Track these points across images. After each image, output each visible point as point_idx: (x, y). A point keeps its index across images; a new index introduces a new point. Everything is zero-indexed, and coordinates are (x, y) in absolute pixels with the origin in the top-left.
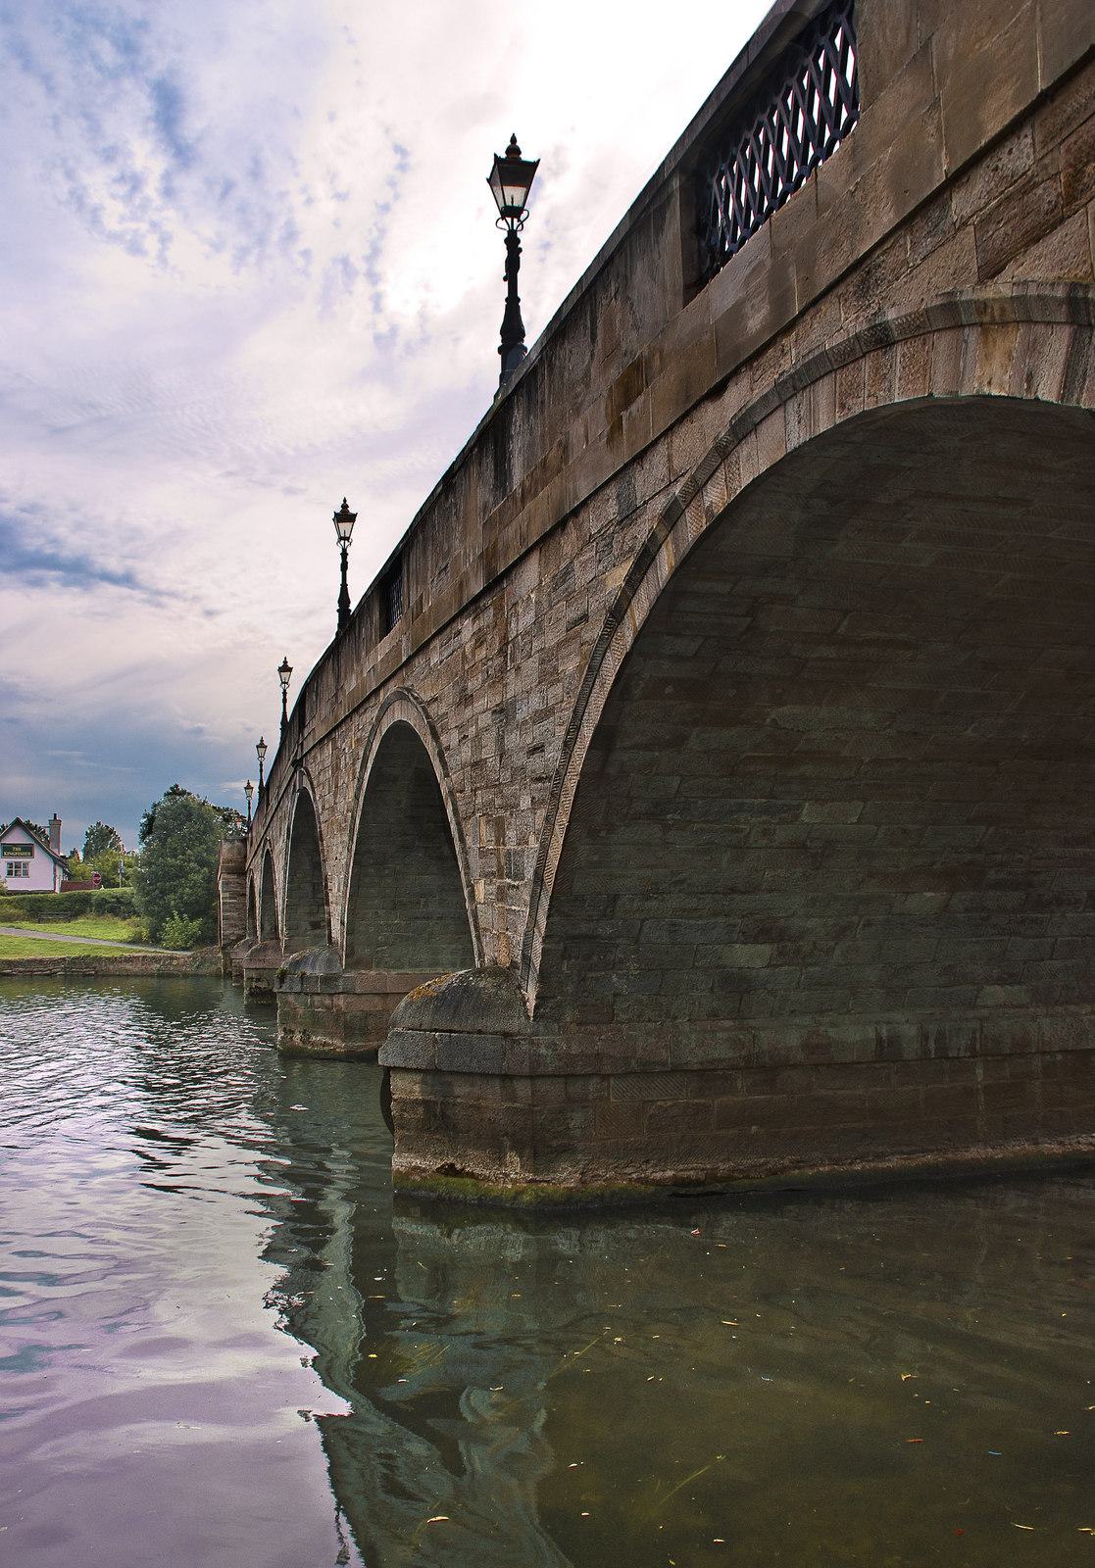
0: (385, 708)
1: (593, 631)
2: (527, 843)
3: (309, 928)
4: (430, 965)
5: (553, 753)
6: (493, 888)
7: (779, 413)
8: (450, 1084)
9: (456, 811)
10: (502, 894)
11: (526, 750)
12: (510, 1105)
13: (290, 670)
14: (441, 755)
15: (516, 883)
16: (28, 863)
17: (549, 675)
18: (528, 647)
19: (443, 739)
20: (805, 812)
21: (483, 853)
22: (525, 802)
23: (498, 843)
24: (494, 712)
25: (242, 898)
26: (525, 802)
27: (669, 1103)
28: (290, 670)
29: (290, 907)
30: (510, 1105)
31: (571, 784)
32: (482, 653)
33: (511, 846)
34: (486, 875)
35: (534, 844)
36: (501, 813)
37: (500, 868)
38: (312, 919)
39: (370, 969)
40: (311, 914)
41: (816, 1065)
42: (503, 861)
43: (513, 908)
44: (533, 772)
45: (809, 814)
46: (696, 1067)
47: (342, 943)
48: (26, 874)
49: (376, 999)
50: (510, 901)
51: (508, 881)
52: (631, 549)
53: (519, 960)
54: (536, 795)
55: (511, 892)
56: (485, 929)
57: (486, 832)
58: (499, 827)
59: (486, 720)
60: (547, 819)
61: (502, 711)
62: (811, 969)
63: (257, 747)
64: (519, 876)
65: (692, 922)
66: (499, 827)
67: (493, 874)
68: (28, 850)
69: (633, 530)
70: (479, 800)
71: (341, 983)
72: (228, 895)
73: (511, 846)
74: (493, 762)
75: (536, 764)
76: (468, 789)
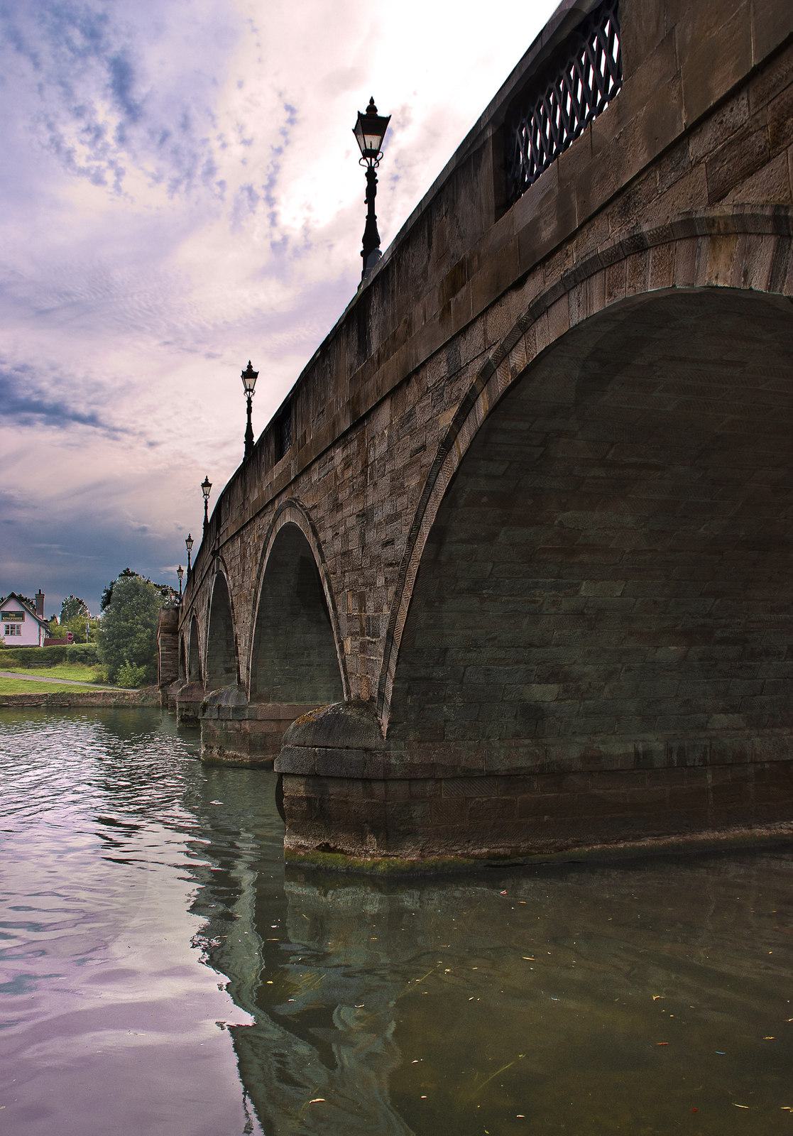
1: (430, 458)
2: (382, 611)
3: (224, 672)
5: (401, 546)
6: (357, 644)
7: (565, 299)
10: (363, 648)
12: (369, 800)
13: (210, 485)
14: (319, 547)
15: (374, 640)
16: (20, 625)
17: (397, 489)
22: (380, 581)
23: (360, 610)
24: (358, 516)
26: (380, 581)
28: (210, 485)
30: (369, 800)
33: (370, 613)
35: (386, 611)
36: (363, 589)
37: (362, 629)
39: (268, 702)
40: (225, 662)
43: (372, 658)
44: (386, 559)
45: (586, 589)
47: (248, 683)
49: (273, 724)
51: (368, 638)
52: (457, 398)
53: (376, 695)
54: (388, 576)
60: (396, 593)
62: (587, 702)
63: (186, 541)
64: (376, 635)
67: (357, 633)
69: (459, 384)
71: (247, 712)
74: (357, 552)
75: (388, 553)
76: (339, 572)
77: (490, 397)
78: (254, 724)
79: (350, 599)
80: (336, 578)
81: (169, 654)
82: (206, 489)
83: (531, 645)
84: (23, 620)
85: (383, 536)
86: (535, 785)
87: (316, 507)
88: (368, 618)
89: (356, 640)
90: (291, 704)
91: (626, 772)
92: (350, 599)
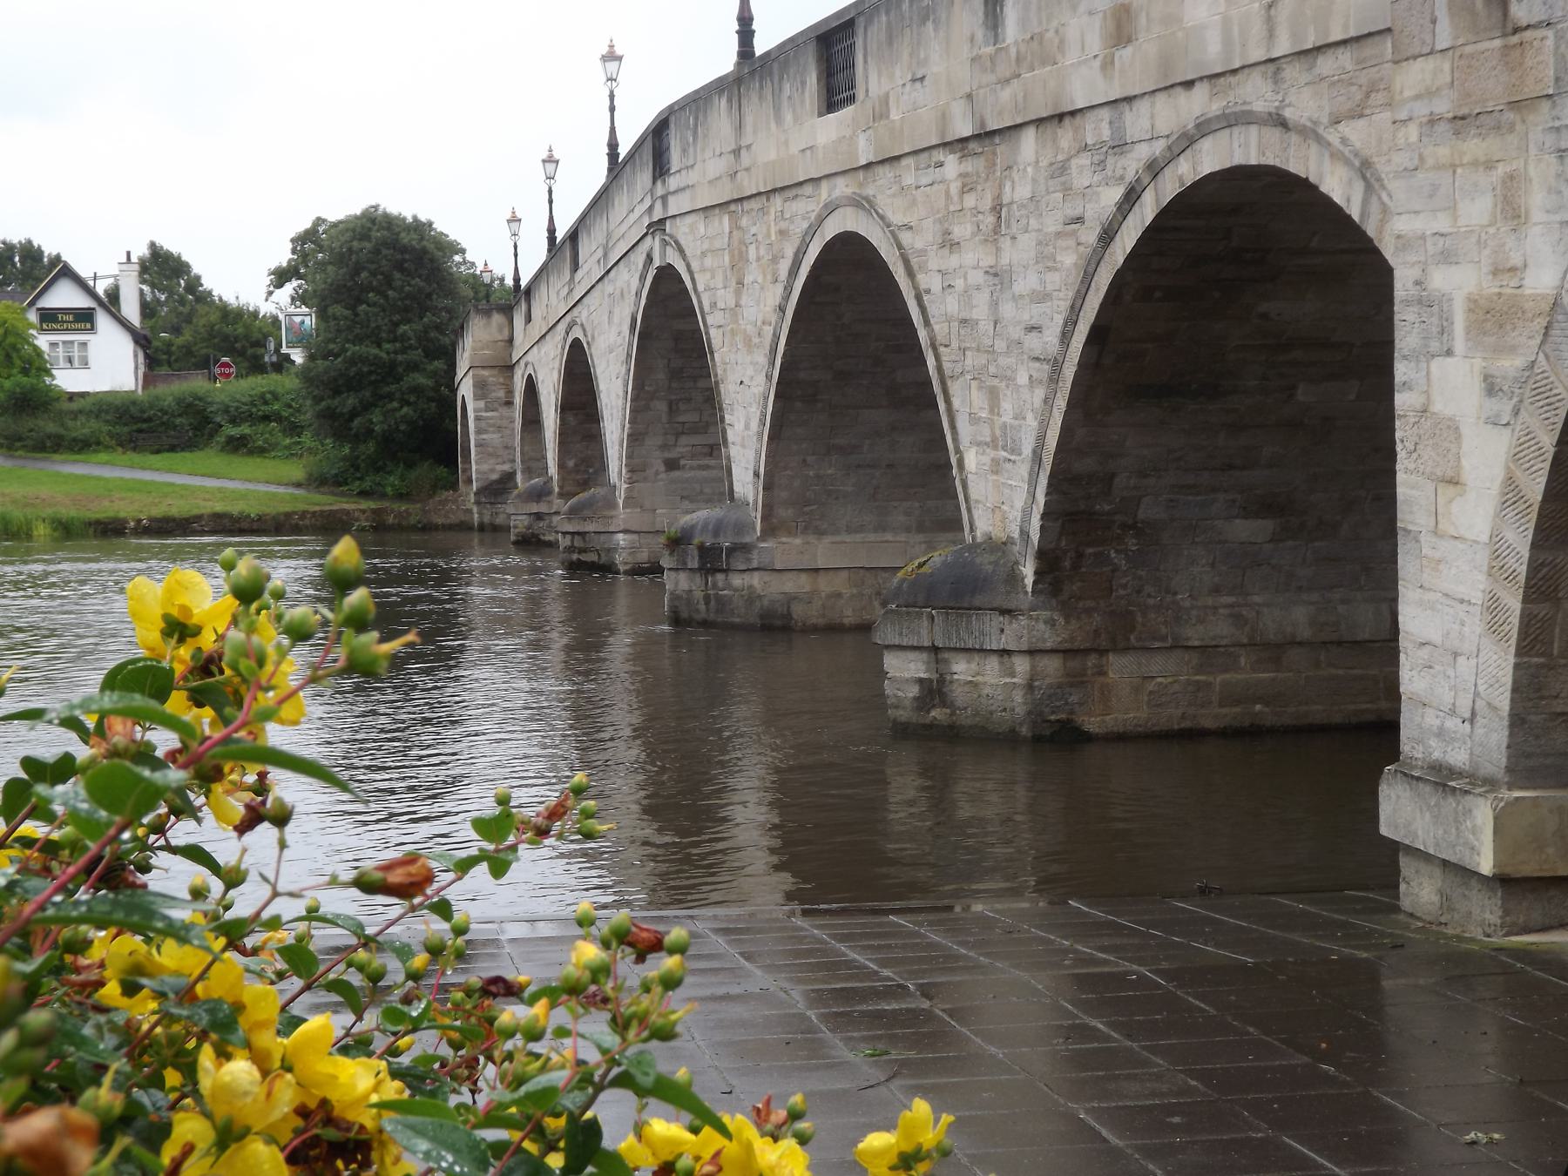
0: (830, 209)
1: (1090, 236)
2: (1024, 418)
3: (662, 468)
4: (876, 530)
5: (1051, 337)
6: (986, 459)
7: (1227, 131)
8: (947, 662)
9: (939, 368)
10: (996, 467)
11: (1023, 326)
12: (1008, 680)
13: (620, 59)
14: (919, 298)
15: (1013, 458)
16: (84, 345)
17: (1046, 261)
18: (1024, 221)
19: (920, 277)
20: (1300, 391)
21: (974, 419)
22: (1022, 379)
23: (992, 411)
24: (987, 272)
25: (504, 411)
26: (1022, 379)
27: (1170, 680)
28: (620, 59)
29: (635, 438)
30: (1008, 680)
31: (1069, 371)
32: (970, 201)
33: (1007, 418)
34: (979, 444)
35: (1032, 422)
36: (996, 382)
37: (994, 440)
38: (667, 455)
39: (796, 535)
40: (664, 447)
41: (1324, 643)
42: (998, 432)
43: (1010, 482)
44: (1031, 350)
45: (1303, 394)
46: (1196, 643)
47: (756, 501)
48: (85, 364)
49: (804, 577)
50: (1006, 475)
51: (1004, 454)
52: (1122, 178)
53: (1016, 535)
54: (1035, 375)
55: (1008, 466)
56: (977, 501)
57: (979, 400)
58: (994, 396)
59: (977, 277)
60: (1046, 401)
61: (996, 275)
62: (1317, 544)
63: (544, 161)
64: (1016, 450)
65: (1190, 498)
66: (994, 396)
67: (987, 444)
68: (84, 319)
69: (1122, 162)
70: (969, 362)
71: (755, 555)
72: (481, 404)
73: (1007, 418)
74: (986, 326)
75: (1033, 343)
76: (955, 344)
77: (1157, 200)
78: (767, 577)
79: (974, 392)
80: (950, 354)
81: (491, 418)
82: (612, 66)
83: (1231, 467)
84: (92, 329)
85: (1026, 317)
86: (1243, 661)
87: (911, 228)
88: (1004, 426)
89: (983, 453)
90: (838, 538)
91: (1378, 645)
92: (974, 392)
